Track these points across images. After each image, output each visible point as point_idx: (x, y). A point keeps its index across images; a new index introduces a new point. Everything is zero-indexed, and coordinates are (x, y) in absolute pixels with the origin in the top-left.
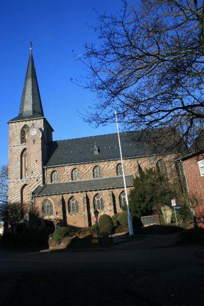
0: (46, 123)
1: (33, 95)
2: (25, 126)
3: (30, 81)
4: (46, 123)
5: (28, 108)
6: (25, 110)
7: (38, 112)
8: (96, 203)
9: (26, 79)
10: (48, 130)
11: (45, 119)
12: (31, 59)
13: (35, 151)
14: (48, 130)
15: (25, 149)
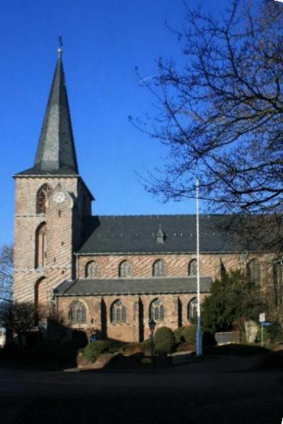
0: (81, 185)
1: (61, 134)
2: (45, 186)
3: (55, 110)
4: (81, 185)
5: (51, 155)
6: (45, 159)
7: (68, 165)
8: (153, 311)
9: (49, 104)
10: (84, 198)
11: (80, 180)
12: (59, 69)
13: (61, 229)
14: (84, 198)
15: (43, 223)
